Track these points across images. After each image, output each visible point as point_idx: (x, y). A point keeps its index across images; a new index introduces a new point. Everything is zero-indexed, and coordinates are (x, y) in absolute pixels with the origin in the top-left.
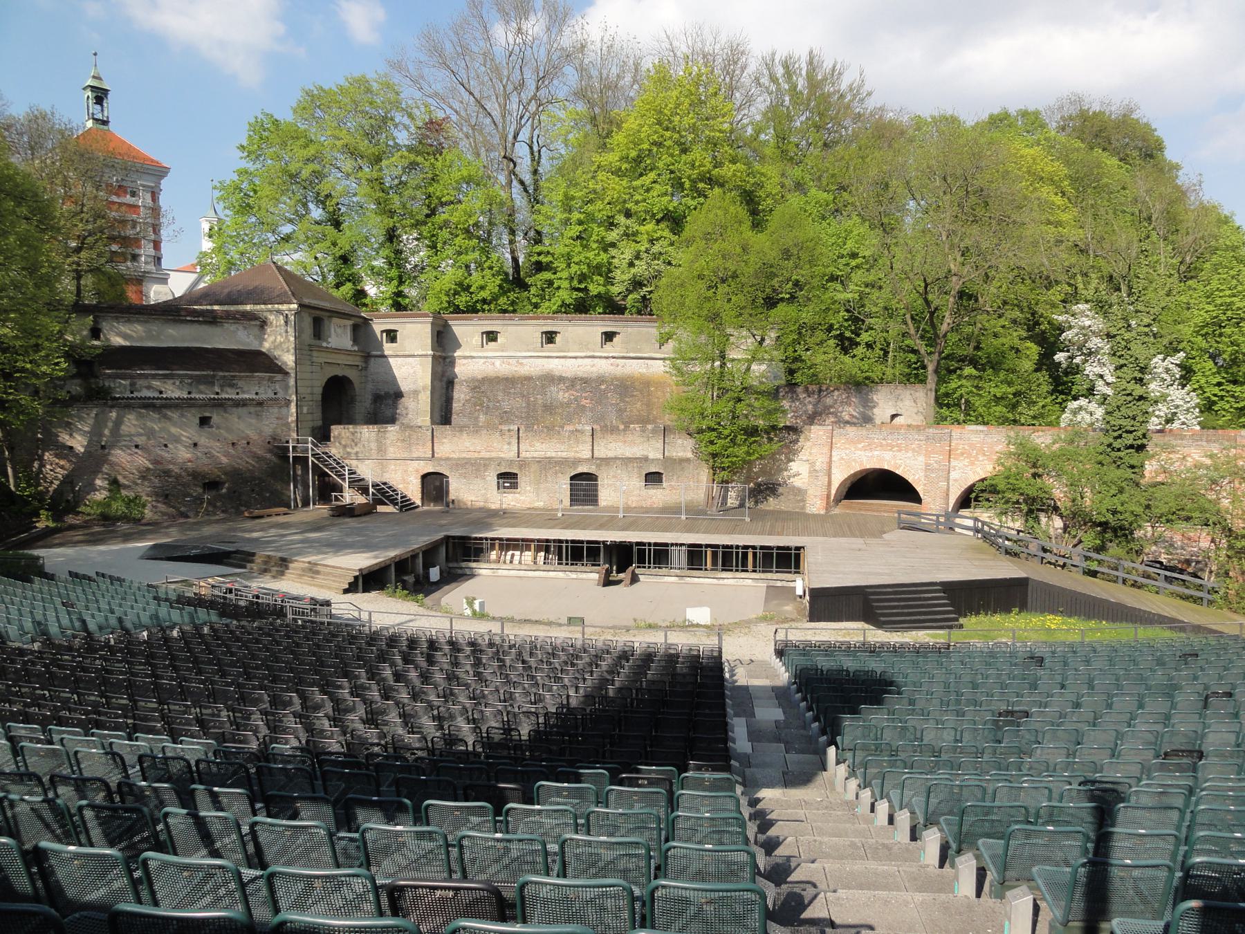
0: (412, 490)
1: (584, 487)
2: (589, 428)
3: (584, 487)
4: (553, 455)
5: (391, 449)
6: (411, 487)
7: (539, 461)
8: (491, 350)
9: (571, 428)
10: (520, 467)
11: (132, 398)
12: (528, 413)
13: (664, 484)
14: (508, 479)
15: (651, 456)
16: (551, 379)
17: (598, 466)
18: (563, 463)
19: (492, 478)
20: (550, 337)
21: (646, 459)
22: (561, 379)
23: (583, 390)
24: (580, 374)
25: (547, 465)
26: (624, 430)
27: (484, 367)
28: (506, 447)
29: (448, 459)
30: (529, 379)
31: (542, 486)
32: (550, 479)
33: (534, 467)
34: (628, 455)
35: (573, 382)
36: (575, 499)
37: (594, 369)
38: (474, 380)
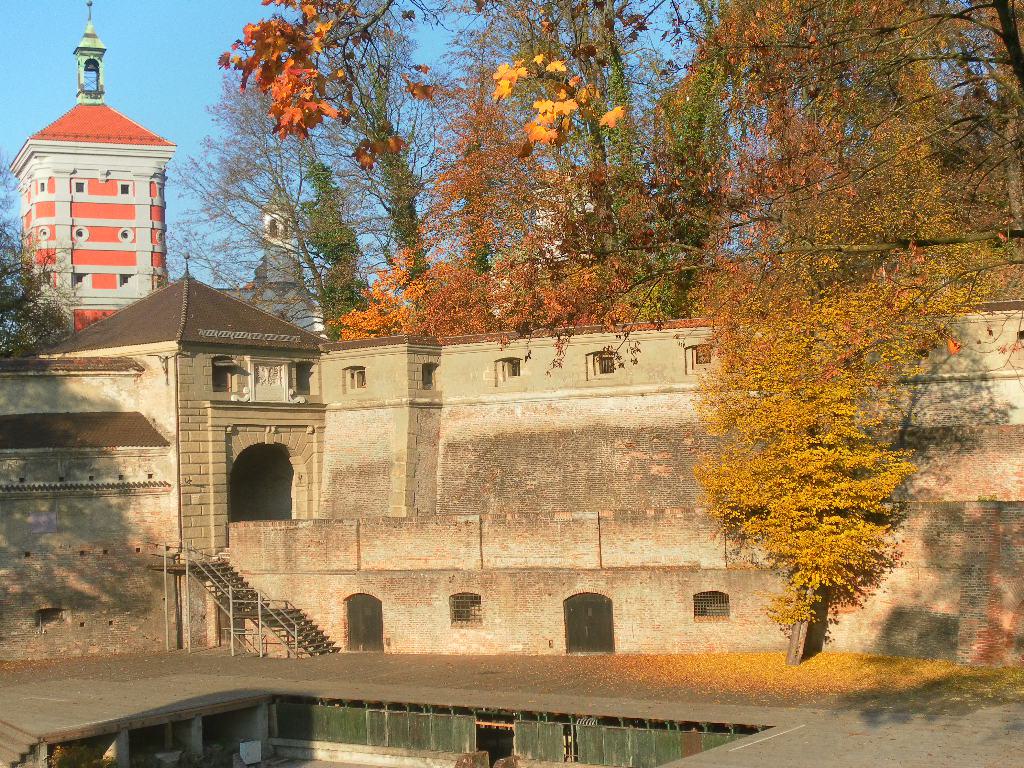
0: (332, 622)
1: (589, 621)
2: (592, 516)
3: (589, 621)
4: (539, 563)
5: (303, 559)
6: (331, 617)
7: (513, 573)
8: (512, 391)
9: (566, 516)
10: (485, 584)
11: (92, 487)
12: (563, 491)
13: (732, 615)
14: (464, 608)
15: (705, 563)
16: (602, 433)
17: (610, 582)
18: (550, 576)
19: (443, 606)
20: (514, 365)
21: (694, 569)
22: (619, 432)
23: (655, 449)
24: (649, 422)
25: (526, 578)
26: (656, 518)
27: (498, 418)
28: (463, 550)
29: (380, 572)
30: (565, 434)
31: (519, 616)
32: (530, 605)
33: (506, 584)
34: (664, 561)
35: (636, 437)
36: (574, 640)
37: (674, 413)
38: (484, 440)
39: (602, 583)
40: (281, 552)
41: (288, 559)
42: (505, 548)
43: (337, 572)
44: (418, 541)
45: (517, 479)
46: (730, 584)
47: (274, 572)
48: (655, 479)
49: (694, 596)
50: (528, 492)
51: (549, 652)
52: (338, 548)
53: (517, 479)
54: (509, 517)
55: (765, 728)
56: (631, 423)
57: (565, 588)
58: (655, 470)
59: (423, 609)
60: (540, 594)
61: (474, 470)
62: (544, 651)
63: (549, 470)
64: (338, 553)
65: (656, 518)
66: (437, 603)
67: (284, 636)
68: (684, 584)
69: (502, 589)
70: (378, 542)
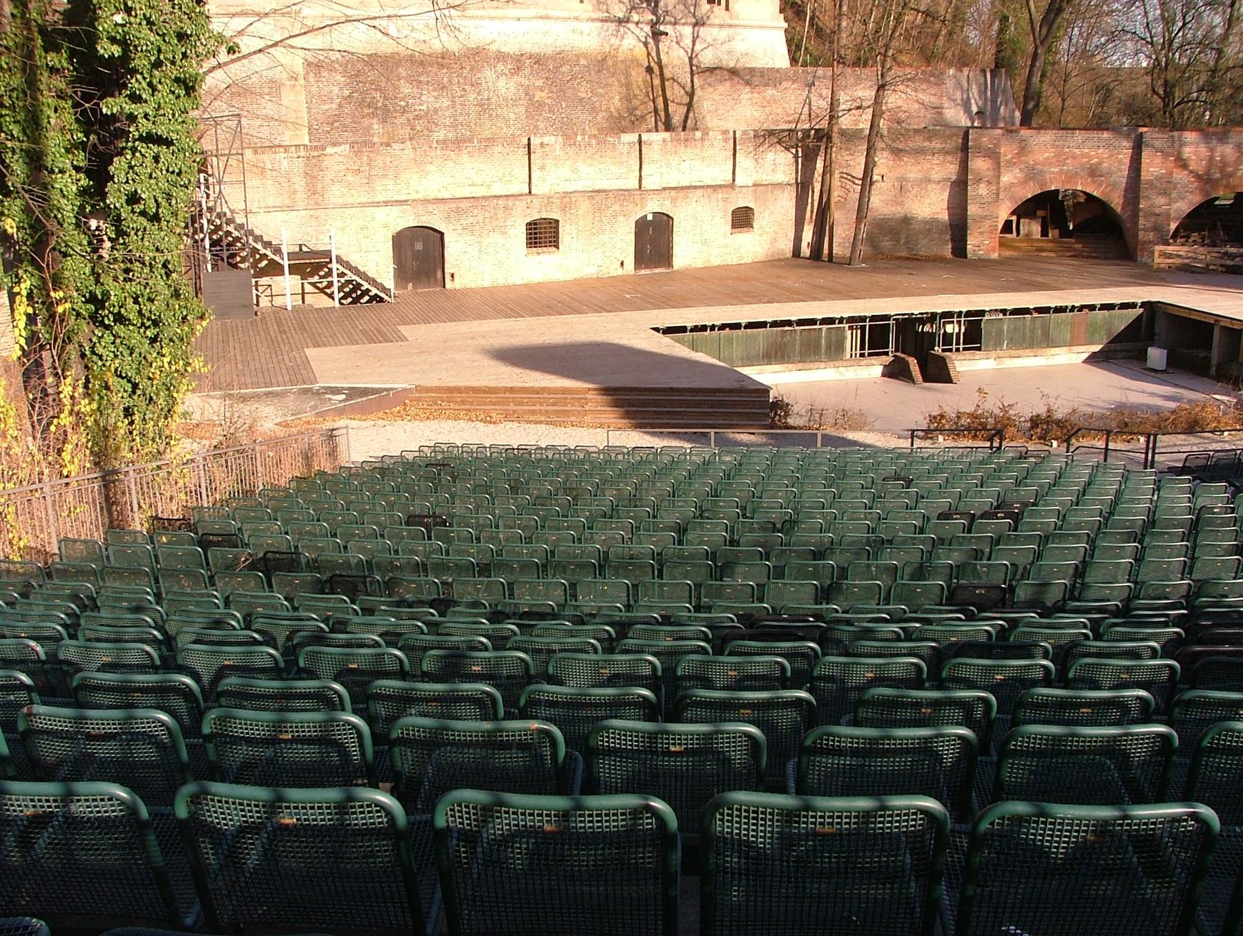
1: (654, 240)
3: (654, 240)
14: (542, 234)
22: (501, 57)
33: (584, 206)
35: (517, 62)
36: (641, 259)
39: (668, 202)
40: (300, 183)
41: (312, 191)
42: (575, 171)
43: (387, 203)
44: (482, 166)
45: (403, 103)
46: (756, 200)
47: (291, 208)
48: (541, 104)
49: (557, 221)
50: (417, 118)
51: (620, 272)
52: (385, 176)
53: (403, 103)
54: (579, 138)
55: (657, 330)
56: (510, 48)
57: (637, 209)
58: (539, 96)
59: (495, 238)
60: (615, 216)
61: (347, 93)
62: (616, 271)
63: (435, 94)
64: (385, 181)
65: (702, 139)
66: (512, 232)
67: (59, 302)
68: (725, 200)
69: (580, 212)
70: (432, 168)
